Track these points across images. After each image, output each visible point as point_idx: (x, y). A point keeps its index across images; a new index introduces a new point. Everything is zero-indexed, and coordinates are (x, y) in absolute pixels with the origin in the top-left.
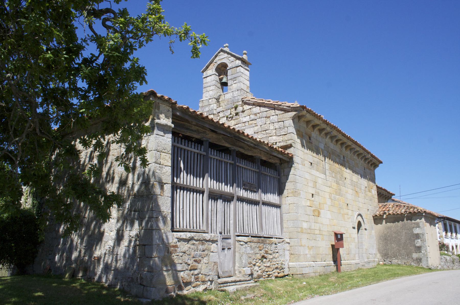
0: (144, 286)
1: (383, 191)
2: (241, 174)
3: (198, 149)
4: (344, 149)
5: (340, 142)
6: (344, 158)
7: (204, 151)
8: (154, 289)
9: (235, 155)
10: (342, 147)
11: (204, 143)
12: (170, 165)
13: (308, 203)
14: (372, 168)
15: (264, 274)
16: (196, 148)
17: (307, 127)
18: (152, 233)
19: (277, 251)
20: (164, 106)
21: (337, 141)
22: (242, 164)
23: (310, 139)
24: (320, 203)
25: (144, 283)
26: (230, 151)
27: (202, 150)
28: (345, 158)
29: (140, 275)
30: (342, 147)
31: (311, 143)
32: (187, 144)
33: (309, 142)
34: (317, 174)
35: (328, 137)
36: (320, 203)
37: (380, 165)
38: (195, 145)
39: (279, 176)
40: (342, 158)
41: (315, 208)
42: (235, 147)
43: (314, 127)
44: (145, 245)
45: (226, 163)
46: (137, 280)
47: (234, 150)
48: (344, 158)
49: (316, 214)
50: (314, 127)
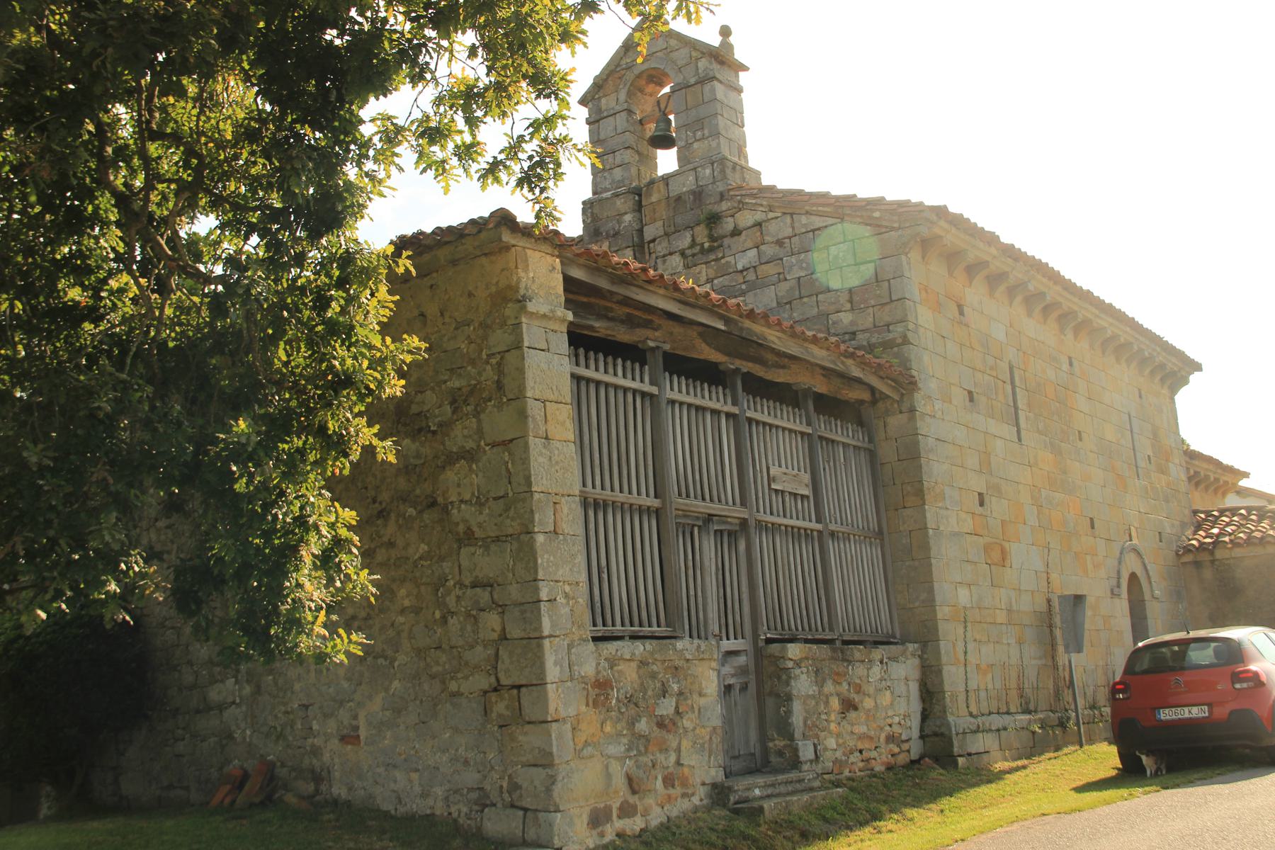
0: (525, 810)
1: (1205, 465)
2: (762, 444)
3: (633, 379)
4: (1070, 335)
5: (1055, 315)
6: (1071, 364)
7: (652, 383)
8: (559, 815)
9: (811, 407)
10: (1062, 330)
11: (648, 355)
12: (572, 437)
13: (968, 525)
14: (1165, 391)
15: (852, 759)
16: (629, 376)
17: (951, 273)
18: (540, 646)
19: (1065, 360)
20: (538, 255)
21: (1046, 310)
22: (762, 412)
23: (961, 313)
24: (1003, 522)
25: (527, 802)
26: (643, 352)
27: (647, 379)
28: (1075, 363)
29: (510, 776)
30: (1062, 330)
31: (967, 326)
32: (592, 363)
33: (960, 323)
34: (994, 427)
35: (1019, 299)
36: (1003, 522)
37: (1195, 378)
38: (710, 392)
39: (870, 441)
40: (1065, 367)
41: (988, 540)
42: (750, 365)
43: (971, 270)
44: (519, 687)
45: (715, 412)
46: (501, 792)
47: (737, 370)
48: (1071, 364)
49: (996, 555)
50: (971, 270)
